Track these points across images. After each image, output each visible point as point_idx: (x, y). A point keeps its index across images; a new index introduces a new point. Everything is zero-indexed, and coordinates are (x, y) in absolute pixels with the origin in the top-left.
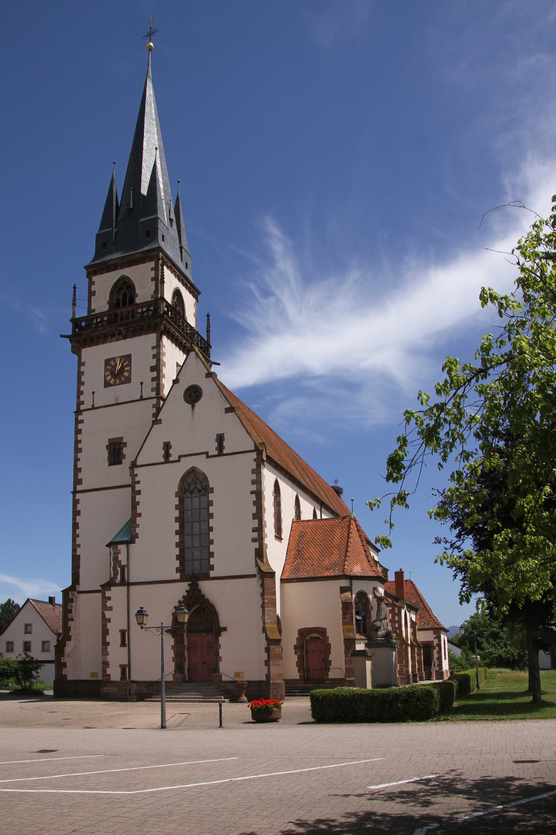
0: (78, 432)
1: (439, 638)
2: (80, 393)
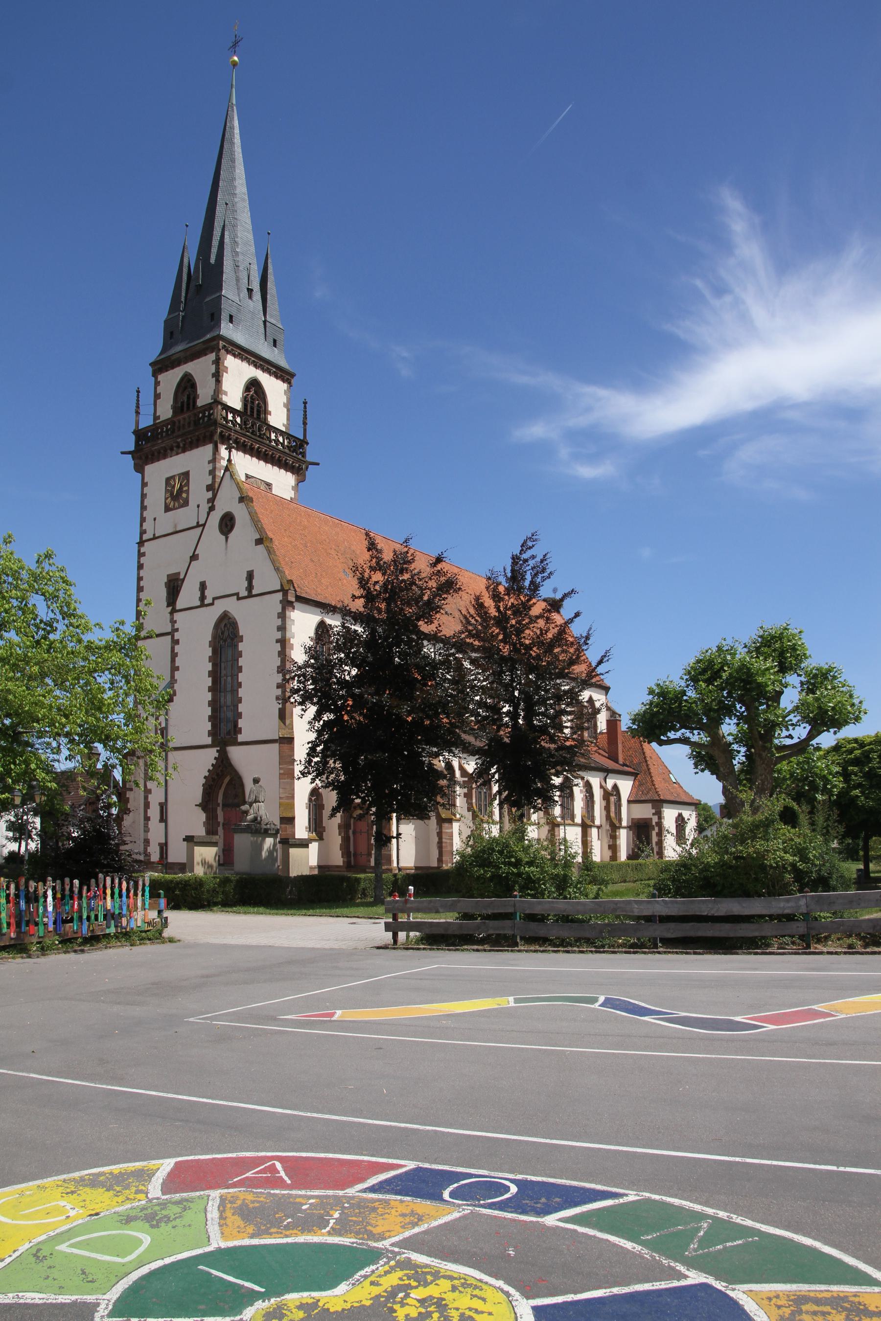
0: (140, 567)
1: (659, 814)
2: (143, 520)
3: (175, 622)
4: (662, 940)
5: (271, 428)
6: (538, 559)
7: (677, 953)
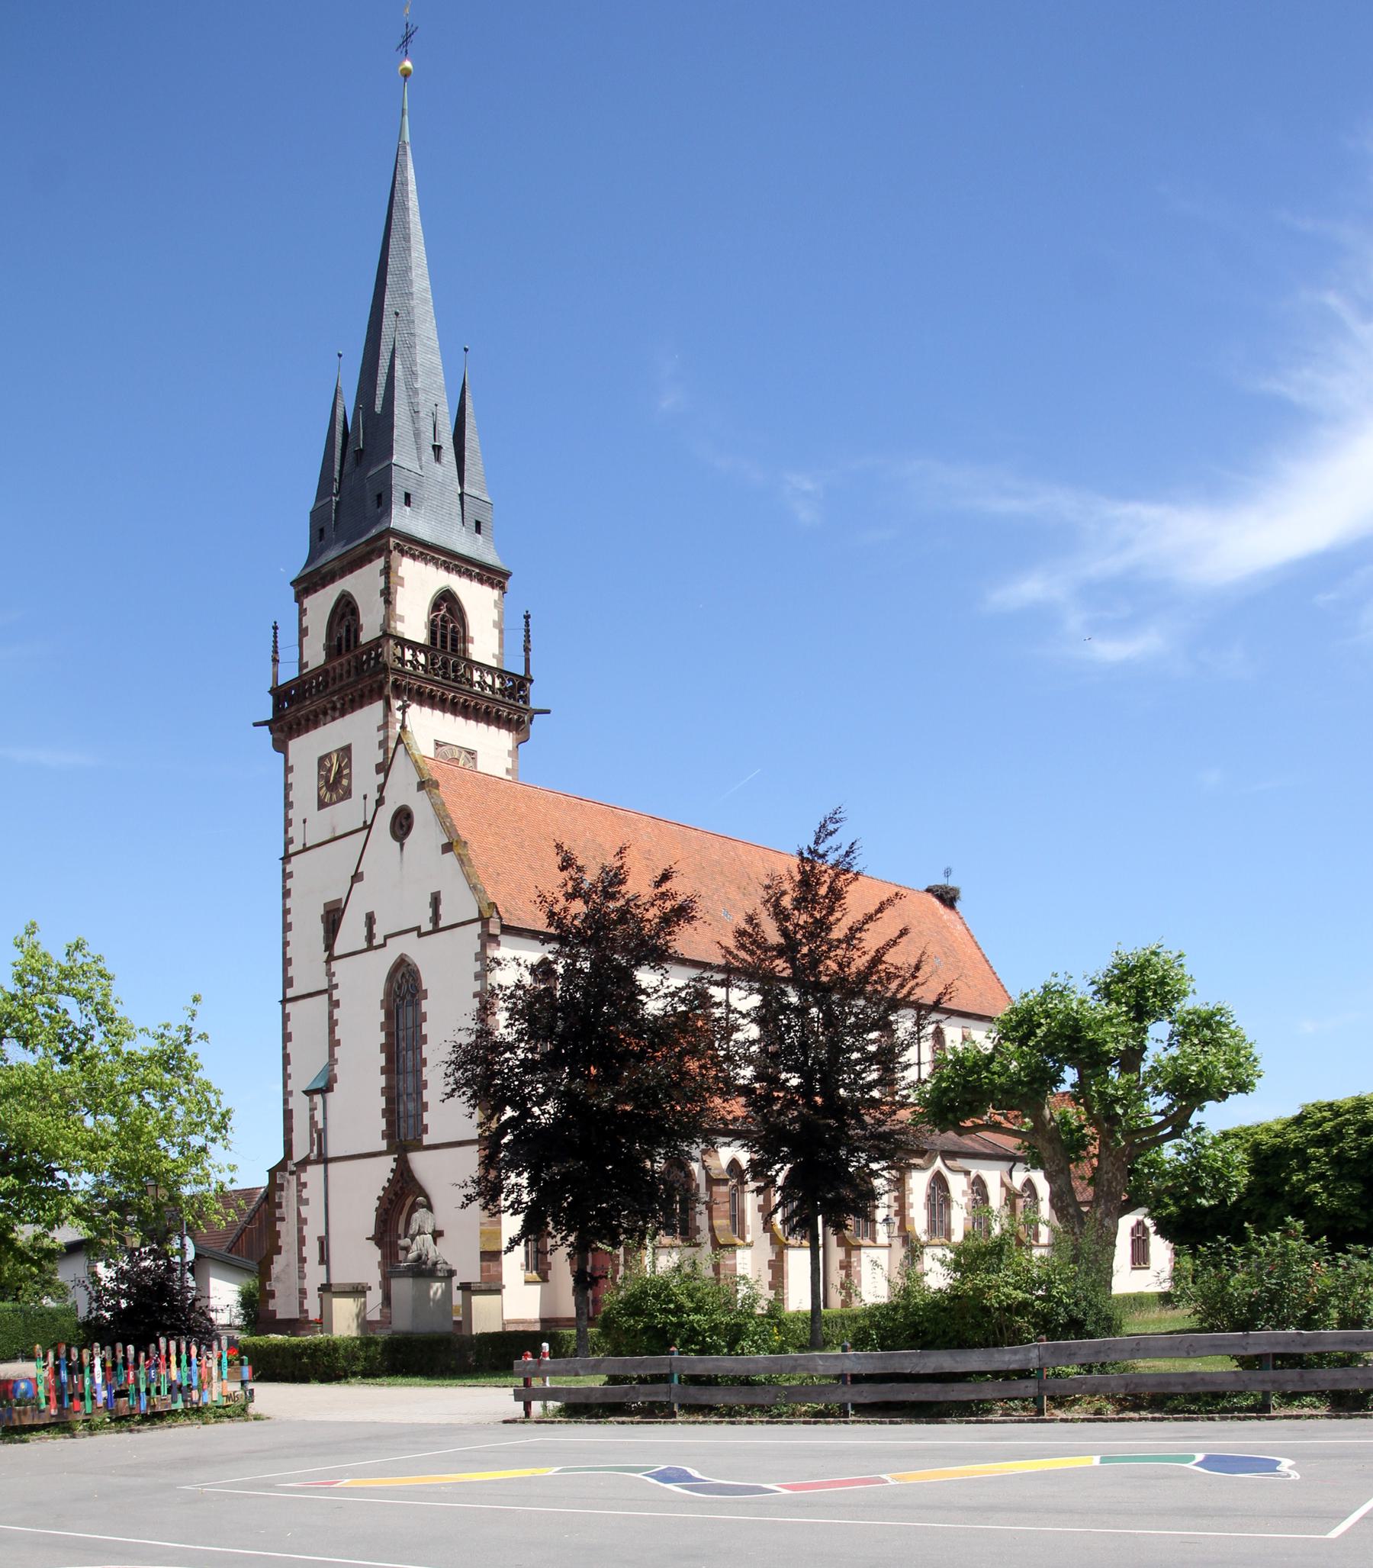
0: (286, 894)
3: (334, 974)
4: (855, 1406)
5: (472, 664)
6: (842, 851)
7: (868, 1423)
